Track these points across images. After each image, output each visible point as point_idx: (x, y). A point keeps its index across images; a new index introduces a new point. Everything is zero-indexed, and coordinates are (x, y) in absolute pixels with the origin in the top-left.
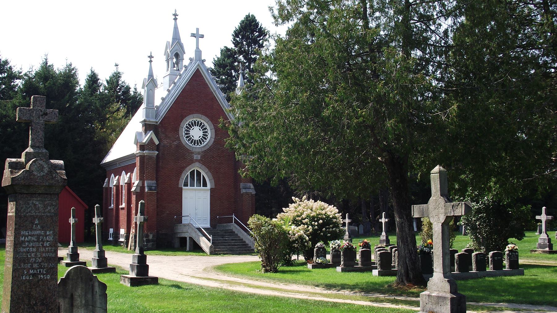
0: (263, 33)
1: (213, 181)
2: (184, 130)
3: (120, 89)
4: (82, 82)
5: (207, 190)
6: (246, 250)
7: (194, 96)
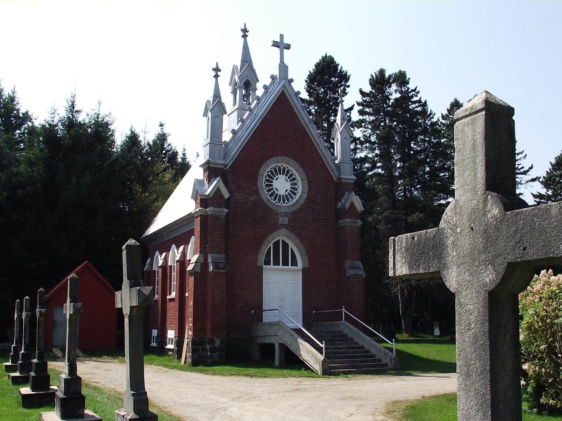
1: (306, 257)
4: (119, 138)
5: (297, 271)
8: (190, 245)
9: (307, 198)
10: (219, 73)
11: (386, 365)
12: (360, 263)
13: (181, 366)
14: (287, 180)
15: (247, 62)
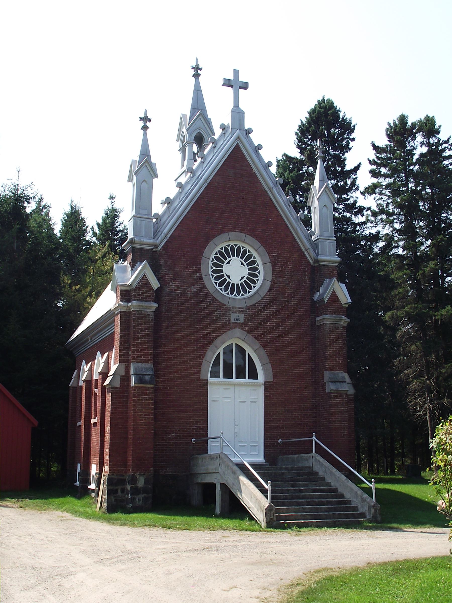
2: (210, 263)
9: (271, 288)
10: (148, 124)
11: (363, 515)
12: (346, 375)
14: (242, 264)
15: (198, 109)
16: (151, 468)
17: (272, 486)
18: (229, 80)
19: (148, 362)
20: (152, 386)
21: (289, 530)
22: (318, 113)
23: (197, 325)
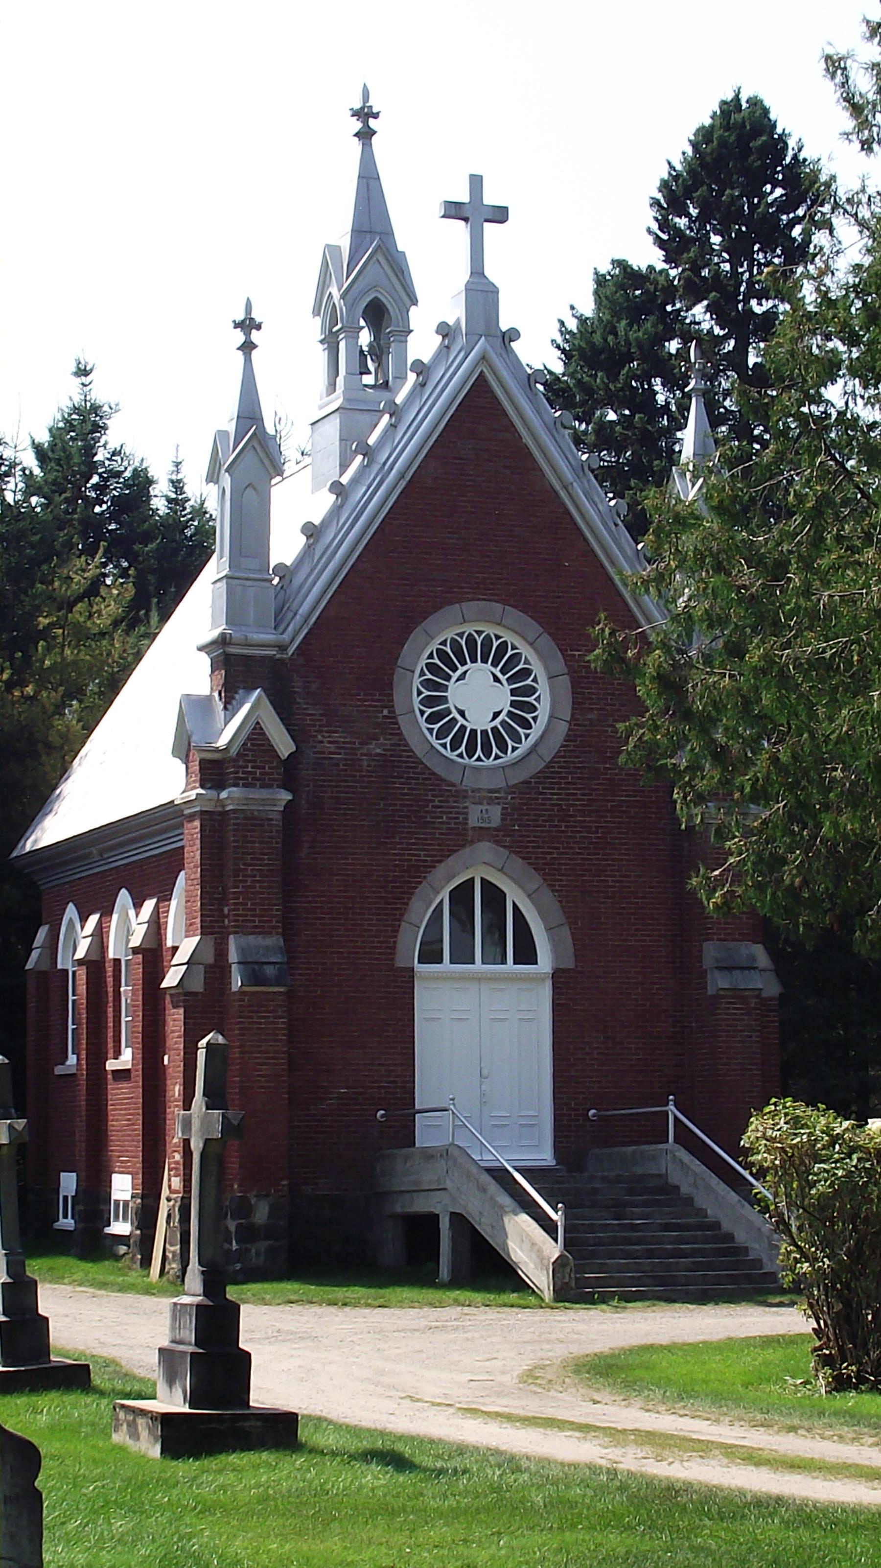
0: (806, 187)
1: (566, 932)
2: (417, 682)
3: (101, 488)
5: (538, 979)
6: (735, 1278)
7: (473, 501)
8: (174, 903)
10: (255, 336)
13: (150, 1284)
16: (283, 1179)
17: (566, 1216)
18: (458, 205)
19: (270, 933)
20: (282, 989)
21: (604, 1307)
22: (719, 144)
23: (386, 838)
